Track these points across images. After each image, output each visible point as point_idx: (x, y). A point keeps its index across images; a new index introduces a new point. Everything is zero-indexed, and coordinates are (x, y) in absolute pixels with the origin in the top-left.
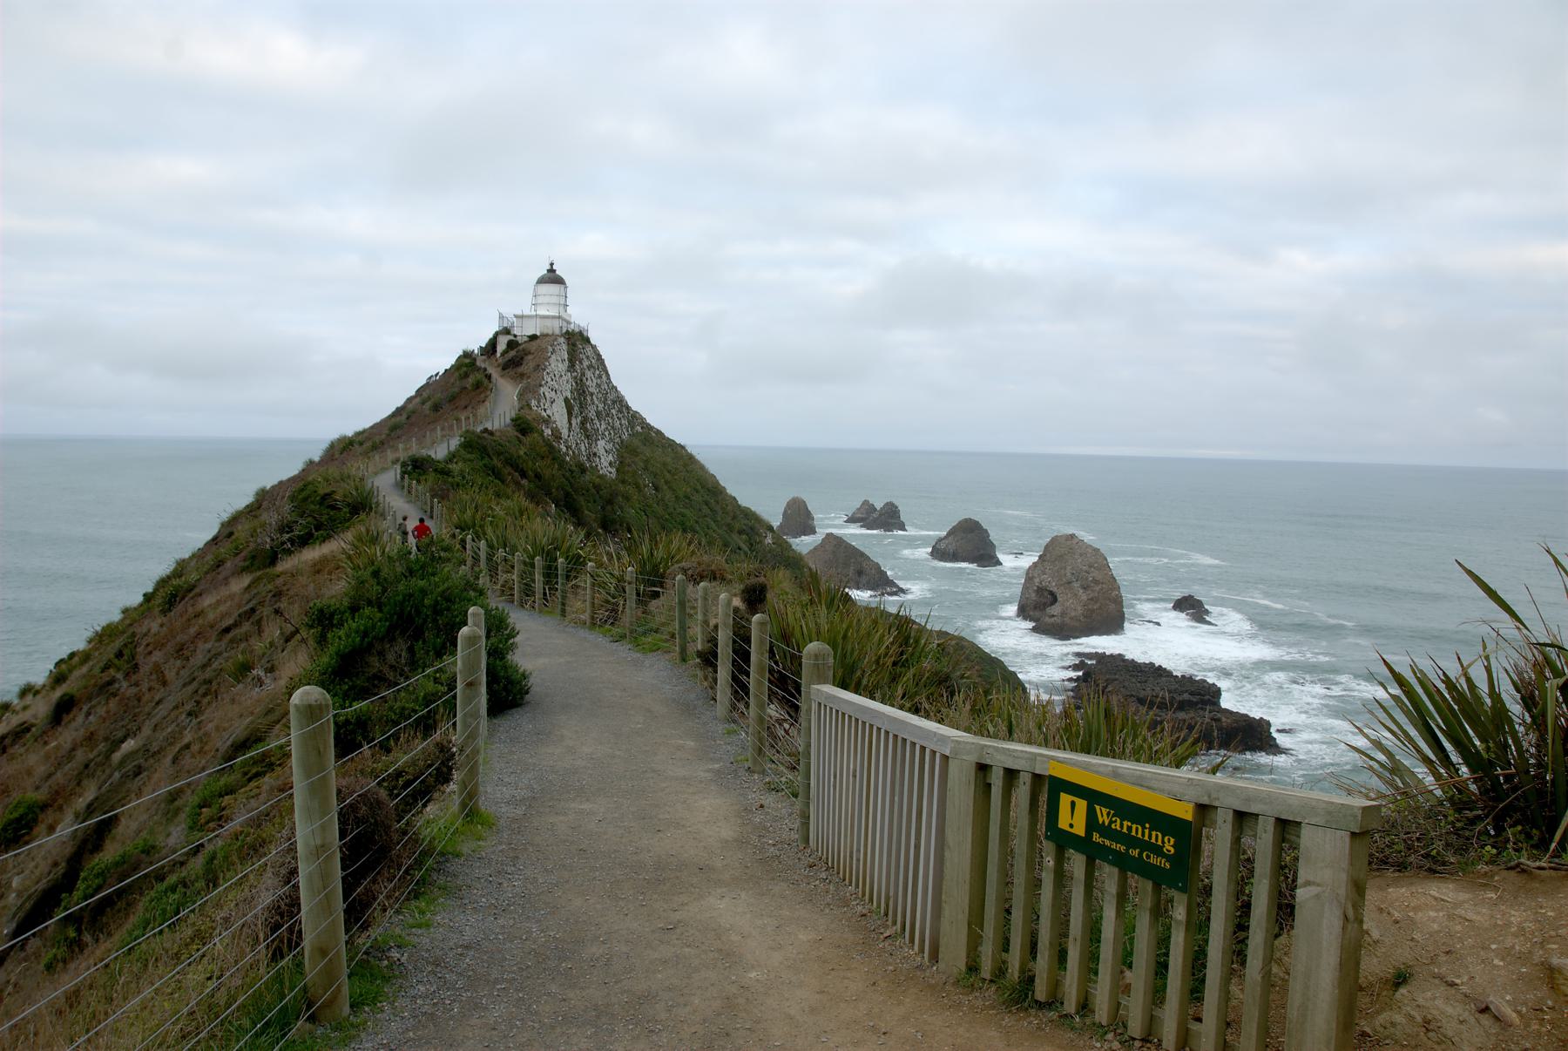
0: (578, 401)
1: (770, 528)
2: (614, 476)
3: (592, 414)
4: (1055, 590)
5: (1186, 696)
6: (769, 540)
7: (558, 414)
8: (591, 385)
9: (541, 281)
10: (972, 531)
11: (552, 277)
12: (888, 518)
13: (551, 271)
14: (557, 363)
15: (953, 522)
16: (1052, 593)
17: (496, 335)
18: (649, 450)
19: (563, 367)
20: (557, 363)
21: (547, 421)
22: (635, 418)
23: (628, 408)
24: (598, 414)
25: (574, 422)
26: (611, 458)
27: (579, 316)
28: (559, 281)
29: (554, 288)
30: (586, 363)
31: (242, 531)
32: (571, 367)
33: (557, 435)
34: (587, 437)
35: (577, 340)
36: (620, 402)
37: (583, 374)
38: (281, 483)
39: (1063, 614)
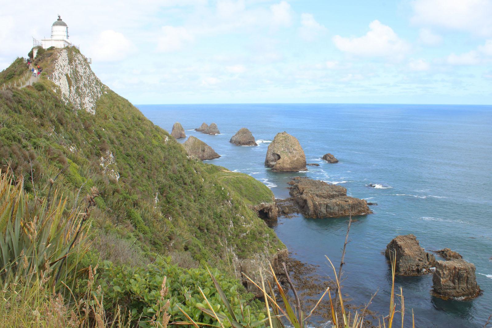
0: (73, 79)
1: (167, 135)
2: (94, 113)
3: (81, 85)
4: (279, 154)
5: (334, 193)
6: (167, 139)
7: (63, 85)
8: (81, 70)
9: (55, 24)
10: (245, 133)
11: (60, 22)
12: (210, 130)
13: (59, 19)
15: (240, 128)
16: (278, 155)
17: (32, 49)
18: (111, 101)
20: (62, 59)
21: (54, 86)
22: (103, 88)
23: (101, 84)
24: (85, 85)
25: (72, 88)
26: (92, 105)
27: (74, 42)
28: (64, 25)
29: (63, 28)
30: (77, 61)
32: (70, 62)
33: (59, 91)
34: (79, 95)
35: (72, 51)
36: (98, 82)
37: (76, 67)
38: (127, 101)
39: (283, 163)
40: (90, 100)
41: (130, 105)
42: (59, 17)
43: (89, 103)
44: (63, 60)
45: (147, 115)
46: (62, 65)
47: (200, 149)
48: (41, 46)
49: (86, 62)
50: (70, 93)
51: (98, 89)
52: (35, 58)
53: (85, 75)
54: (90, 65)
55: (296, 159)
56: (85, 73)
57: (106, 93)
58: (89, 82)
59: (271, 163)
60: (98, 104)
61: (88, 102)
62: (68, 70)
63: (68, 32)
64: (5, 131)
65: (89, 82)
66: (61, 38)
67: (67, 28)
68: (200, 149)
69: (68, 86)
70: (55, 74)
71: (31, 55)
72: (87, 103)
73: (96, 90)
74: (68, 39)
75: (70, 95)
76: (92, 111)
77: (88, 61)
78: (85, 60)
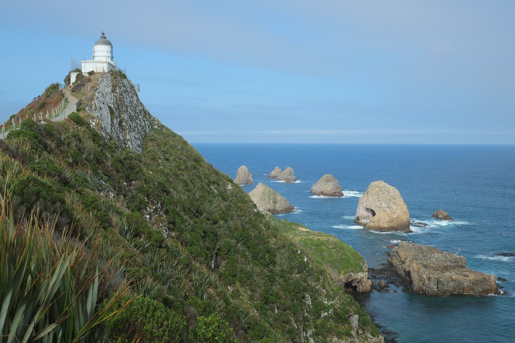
4: (374, 209)
6: (230, 187)
14: (105, 87)
19: (109, 90)
23: (150, 116)
24: (131, 118)
25: (115, 121)
27: (120, 66)
31: (125, 81)
35: (117, 76)
36: (146, 113)
42: (103, 34)
47: (272, 200)
55: (395, 216)
59: (362, 221)
60: (145, 138)
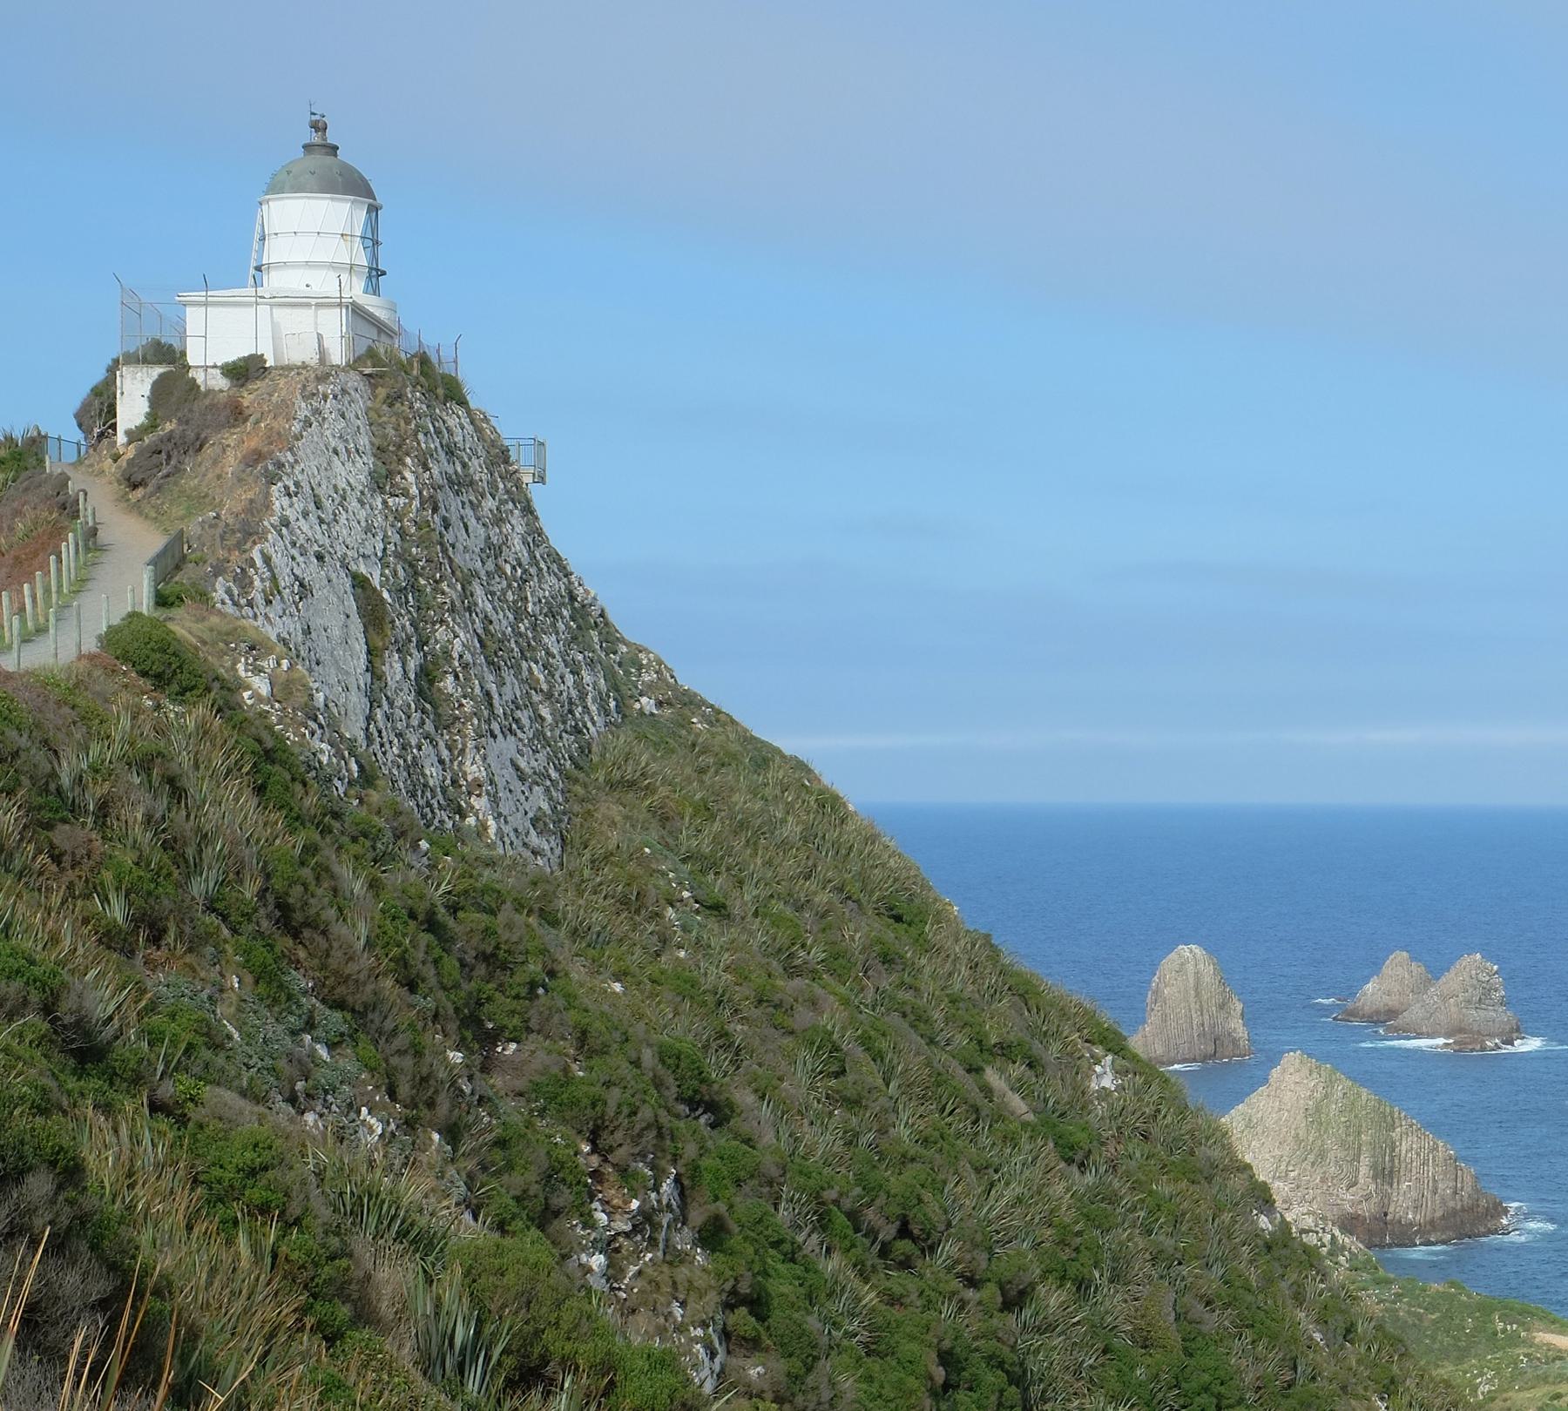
3: (456, 639)
18: (683, 782)
25: (393, 669)
29: (340, 213)
36: (585, 621)
40: (522, 764)
41: (829, 803)
42: (319, 127)
43: (517, 785)
44: (336, 452)
45: (962, 906)
46: (321, 492)
47: (1365, 1160)
48: (176, 345)
49: (500, 474)
50: (373, 703)
51: (587, 678)
52: (134, 436)
53: (490, 566)
54: (536, 493)
56: (494, 550)
57: (647, 704)
58: (518, 619)
60: (577, 779)
61: (509, 773)
62: (369, 529)
63: (376, 243)
64: (109, 938)
65: (518, 619)
66: (325, 284)
67: (374, 209)
68: (1365, 1160)
69: (360, 647)
70: (267, 560)
71: (99, 410)
72: (501, 783)
73: (570, 679)
74: (376, 292)
75: (370, 718)
76: (534, 840)
77: (523, 462)
78: (500, 456)
